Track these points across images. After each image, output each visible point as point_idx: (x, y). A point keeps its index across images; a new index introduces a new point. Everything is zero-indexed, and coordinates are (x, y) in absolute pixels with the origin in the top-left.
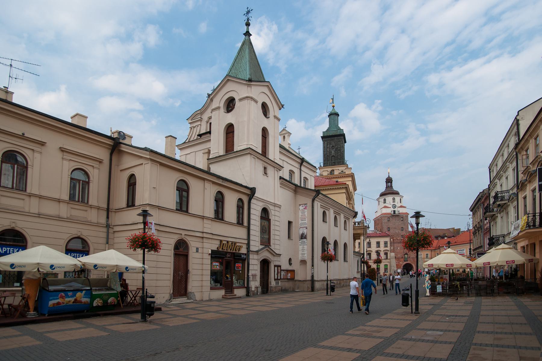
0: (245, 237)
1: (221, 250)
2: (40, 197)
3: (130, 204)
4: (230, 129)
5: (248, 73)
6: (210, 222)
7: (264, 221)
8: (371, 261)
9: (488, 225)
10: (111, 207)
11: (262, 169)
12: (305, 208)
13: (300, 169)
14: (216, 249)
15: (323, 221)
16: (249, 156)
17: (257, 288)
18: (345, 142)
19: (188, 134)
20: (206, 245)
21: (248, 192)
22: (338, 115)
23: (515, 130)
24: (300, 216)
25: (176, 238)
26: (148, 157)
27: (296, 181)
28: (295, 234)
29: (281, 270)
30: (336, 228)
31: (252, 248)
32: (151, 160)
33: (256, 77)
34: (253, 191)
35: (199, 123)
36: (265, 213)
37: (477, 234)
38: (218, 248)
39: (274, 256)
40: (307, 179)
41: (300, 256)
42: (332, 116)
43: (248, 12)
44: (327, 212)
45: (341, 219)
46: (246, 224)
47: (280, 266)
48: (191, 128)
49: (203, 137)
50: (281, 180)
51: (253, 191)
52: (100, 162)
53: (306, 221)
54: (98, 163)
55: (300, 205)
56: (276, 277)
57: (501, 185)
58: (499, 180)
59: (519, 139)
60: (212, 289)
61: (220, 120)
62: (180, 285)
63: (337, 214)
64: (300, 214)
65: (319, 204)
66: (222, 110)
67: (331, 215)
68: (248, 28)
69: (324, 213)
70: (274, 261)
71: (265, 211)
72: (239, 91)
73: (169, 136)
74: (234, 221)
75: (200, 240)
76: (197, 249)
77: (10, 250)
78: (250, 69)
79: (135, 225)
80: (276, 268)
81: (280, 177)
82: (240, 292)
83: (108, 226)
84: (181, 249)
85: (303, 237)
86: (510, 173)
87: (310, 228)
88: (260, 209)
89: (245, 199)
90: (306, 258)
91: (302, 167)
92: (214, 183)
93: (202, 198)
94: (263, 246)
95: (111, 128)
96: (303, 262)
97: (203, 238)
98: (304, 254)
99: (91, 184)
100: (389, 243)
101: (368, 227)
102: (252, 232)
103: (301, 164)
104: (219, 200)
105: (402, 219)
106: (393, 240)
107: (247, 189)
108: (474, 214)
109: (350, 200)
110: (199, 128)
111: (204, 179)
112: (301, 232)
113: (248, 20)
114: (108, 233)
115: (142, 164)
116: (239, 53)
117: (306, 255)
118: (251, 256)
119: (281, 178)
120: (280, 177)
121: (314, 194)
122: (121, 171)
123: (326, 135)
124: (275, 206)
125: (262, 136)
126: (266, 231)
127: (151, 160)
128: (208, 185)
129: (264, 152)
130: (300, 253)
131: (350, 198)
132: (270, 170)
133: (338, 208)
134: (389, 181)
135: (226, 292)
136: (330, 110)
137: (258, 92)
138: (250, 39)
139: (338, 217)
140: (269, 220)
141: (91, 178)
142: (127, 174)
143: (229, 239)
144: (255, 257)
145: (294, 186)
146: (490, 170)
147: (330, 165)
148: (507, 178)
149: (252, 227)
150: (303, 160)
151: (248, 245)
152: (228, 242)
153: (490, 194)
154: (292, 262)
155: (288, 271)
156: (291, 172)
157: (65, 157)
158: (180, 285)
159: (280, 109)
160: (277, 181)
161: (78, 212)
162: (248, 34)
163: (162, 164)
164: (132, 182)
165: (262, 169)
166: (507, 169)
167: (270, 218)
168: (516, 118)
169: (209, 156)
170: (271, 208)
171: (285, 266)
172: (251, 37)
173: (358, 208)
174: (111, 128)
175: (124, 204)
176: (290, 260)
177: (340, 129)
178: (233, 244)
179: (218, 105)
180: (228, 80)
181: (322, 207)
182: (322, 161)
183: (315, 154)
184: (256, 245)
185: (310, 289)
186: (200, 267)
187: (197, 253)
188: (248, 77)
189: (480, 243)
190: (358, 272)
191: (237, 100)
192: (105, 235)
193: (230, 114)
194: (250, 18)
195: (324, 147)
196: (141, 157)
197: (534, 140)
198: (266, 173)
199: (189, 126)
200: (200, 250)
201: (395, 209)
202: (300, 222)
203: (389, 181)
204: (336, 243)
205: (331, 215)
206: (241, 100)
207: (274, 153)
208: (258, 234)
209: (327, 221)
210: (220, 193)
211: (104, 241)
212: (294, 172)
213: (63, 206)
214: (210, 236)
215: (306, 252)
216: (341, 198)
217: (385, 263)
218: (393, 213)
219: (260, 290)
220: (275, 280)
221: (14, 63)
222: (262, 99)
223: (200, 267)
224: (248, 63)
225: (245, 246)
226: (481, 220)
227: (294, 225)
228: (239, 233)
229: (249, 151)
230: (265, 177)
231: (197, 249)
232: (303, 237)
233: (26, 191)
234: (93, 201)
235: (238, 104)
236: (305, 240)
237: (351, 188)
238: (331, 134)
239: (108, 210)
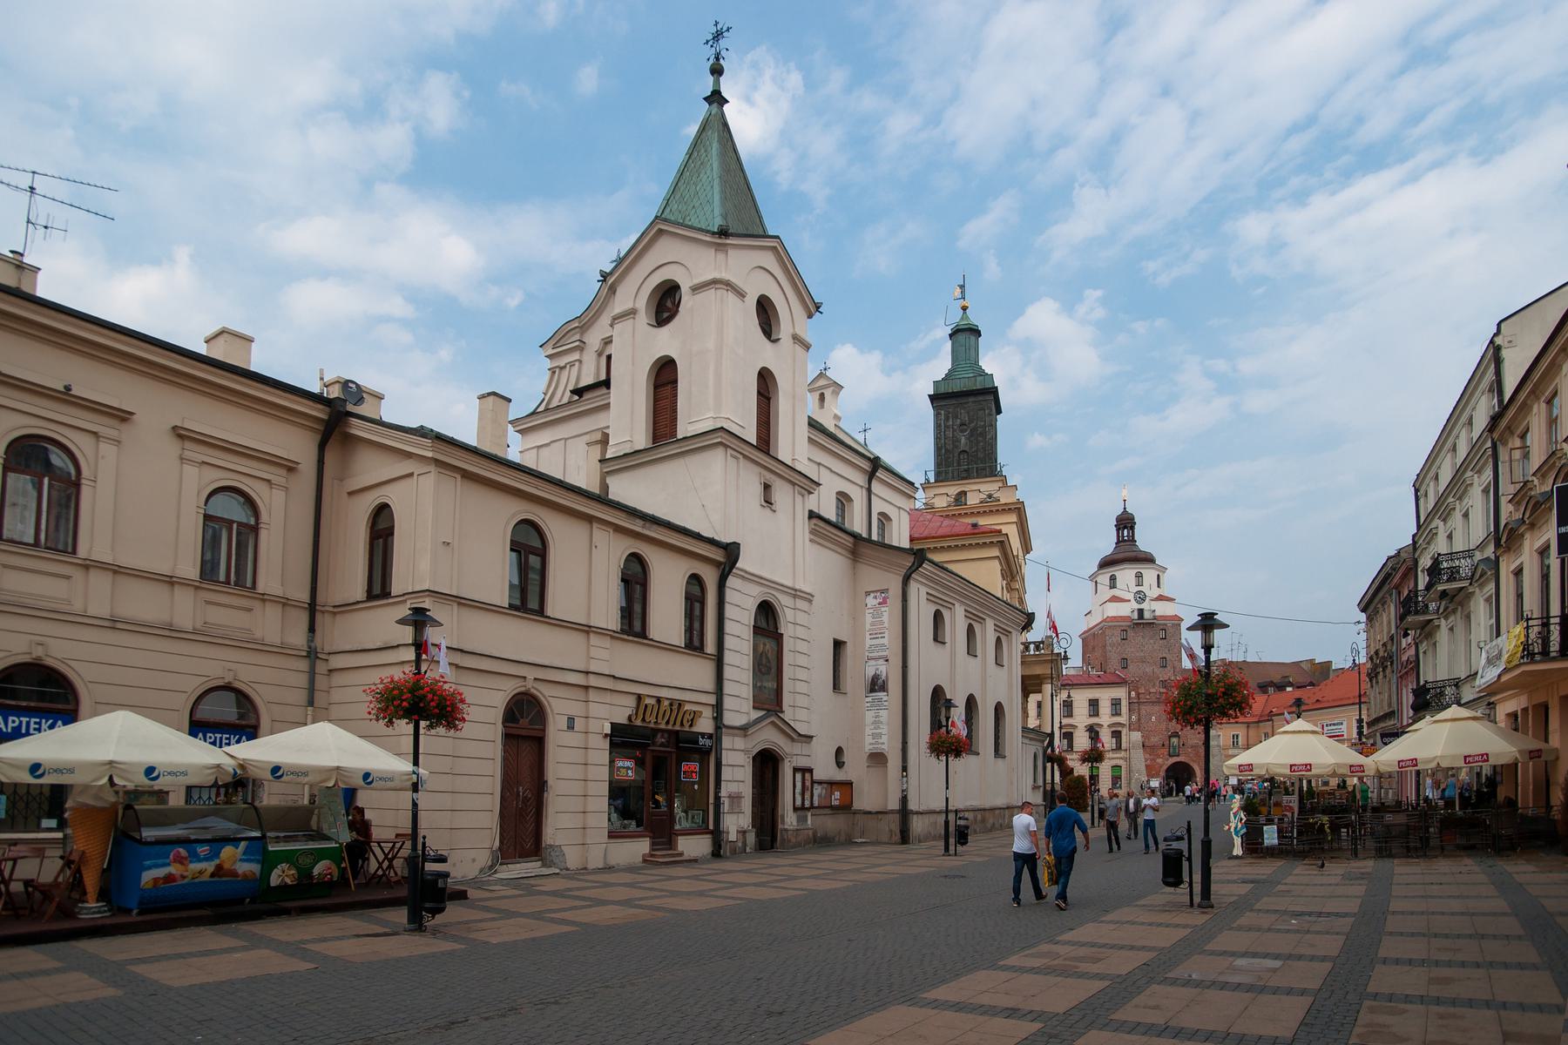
0: (709, 685)
1: (638, 723)
2: (117, 570)
3: (377, 590)
4: (665, 374)
5: (717, 212)
6: (607, 642)
8: (1075, 756)
9: (1412, 651)
10: (320, 599)
11: (758, 490)
12: (884, 602)
13: (869, 491)
14: (625, 721)
15: (936, 639)
16: (720, 451)
17: (744, 832)
18: (999, 411)
19: (543, 387)
20: (595, 709)
21: (718, 555)
22: (977, 333)
24: (868, 627)
25: (510, 688)
26: (430, 454)
28: (855, 678)
29: (813, 782)
30: (971, 659)
31: (730, 719)
32: (437, 462)
33: (741, 222)
34: (731, 552)
35: (576, 356)
37: (1380, 676)
38: (630, 718)
40: (888, 518)
41: (869, 740)
42: (961, 337)
43: (718, 36)
44: (946, 613)
45: (987, 634)
46: (710, 647)
47: (811, 771)
48: (553, 371)
49: (587, 396)
50: (815, 521)
51: (731, 552)
52: (291, 468)
53: (885, 641)
54: (283, 472)
55: (868, 593)
56: (799, 803)
57: (1450, 537)
58: (1444, 520)
60: (612, 835)
61: (636, 348)
62: (522, 824)
63: (973, 620)
64: (869, 619)
65: (924, 590)
66: (644, 318)
67: (957, 622)
68: (717, 83)
69: (938, 616)
70: (793, 756)
71: (766, 611)
72: (690, 264)
74: (678, 639)
75: (580, 694)
76: (571, 720)
77: (28, 724)
78: (724, 199)
79: (390, 652)
80: (799, 776)
81: (811, 512)
82: (693, 846)
83: (312, 655)
84: (524, 722)
85: (876, 685)
86: (1476, 501)
87: (896, 661)
88: (752, 605)
89: (710, 577)
90: (885, 748)
92: (618, 529)
94: (761, 713)
95: (321, 371)
96: (878, 758)
97: (586, 688)
98: (880, 735)
99: (263, 534)
100: (1124, 703)
101: (1066, 658)
102: (728, 672)
103: (871, 476)
104: (635, 579)
106: (1138, 694)
107: (714, 548)
108: (1370, 619)
110: (575, 369)
111: (590, 519)
112: (870, 672)
113: (717, 59)
114: (312, 674)
115: (411, 475)
117: (884, 739)
118: (727, 742)
119: (812, 515)
120: (811, 512)
121: (908, 561)
122: (350, 494)
123: (942, 390)
124: (795, 596)
125: (759, 393)
126: (770, 669)
127: (437, 462)
128: (601, 536)
129: (765, 441)
130: (868, 731)
131: (1011, 572)
132: (782, 493)
133: (979, 602)
134: (1125, 523)
135: (653, 844)
136: (955, 317)
137: (745, 267)
139: (977, 627)
140: (778, 638)
141: (264, 517)
142: (368, 502)
143: (663, 693)
144: (739, 743)
145: (851, 539)
146: (1417, 491)
147: (953, 479)
148: (1466, 515)
149: (729, 657)
150: (876, 464)
151: (718, 708)
152: (659, 700)
153: (1416, 562)
155: (832, 784)
156: (843, 499)
157: (187, 454)
158: (522, 824)
159: (810, 316)
160: (803, 525)
161: (226, 613)
162: (716, 98)
163: (467, 476)
164: (381, 528)
165: (759, 489)
166: (1465, 491)
167: (782, 631)
169: (604, 451)
170: (783, 602)
171: (824, 769)
172: (726, 108)
174: (321, 371)
175: (359, 592)
176: (839, 751)
177: (982, 373)
178: (675, 707)
179: (630, 305)
180: (661, 231)
181: (931, 598)
183: (911, 447)
184: (739, 708)
185: (897, 837)
186: (580, 774)
187: (570, 734)
188: (717, 223)
189: (1390, 705)
190: (1035, 788)
191: (685, 288)
192: (303, 680)
193: (665, 330)
194: (724, 53)
195: (937, 426)
196: (409, 455)
198: (768, 502)
199: (548, 364)
200: (578, 724)
201: (1144, 606)
202: (868, 642)
203: (1125, 523)
204: (971, 703)
205: (957, 622)
206: (696, 289)
207: (792, 444)
209: (947, 640)
210: (635, 558)
211: (301, 696)
212: (849, 499)
213: (184, 598)
214: (609, 684)
215: (884, 730)
216: (986, 573)
218: (1136, 616)
219: (751, 838)
220: (795, 809)
221: (39, 184)
222: (758, 285)
223: (580, 774)
224: (716, 182)
225: (708, 713)
226: (1392, 638)
227: (849, 650)
228: (692, 675)
229: (720, 438)
231: (571, 720)
232: (876, 685)
233: (74, 552)
234: (268, 581)
235: (687, 300)
236: (881, 694)
238: (957, 387)
239: (312, 608)
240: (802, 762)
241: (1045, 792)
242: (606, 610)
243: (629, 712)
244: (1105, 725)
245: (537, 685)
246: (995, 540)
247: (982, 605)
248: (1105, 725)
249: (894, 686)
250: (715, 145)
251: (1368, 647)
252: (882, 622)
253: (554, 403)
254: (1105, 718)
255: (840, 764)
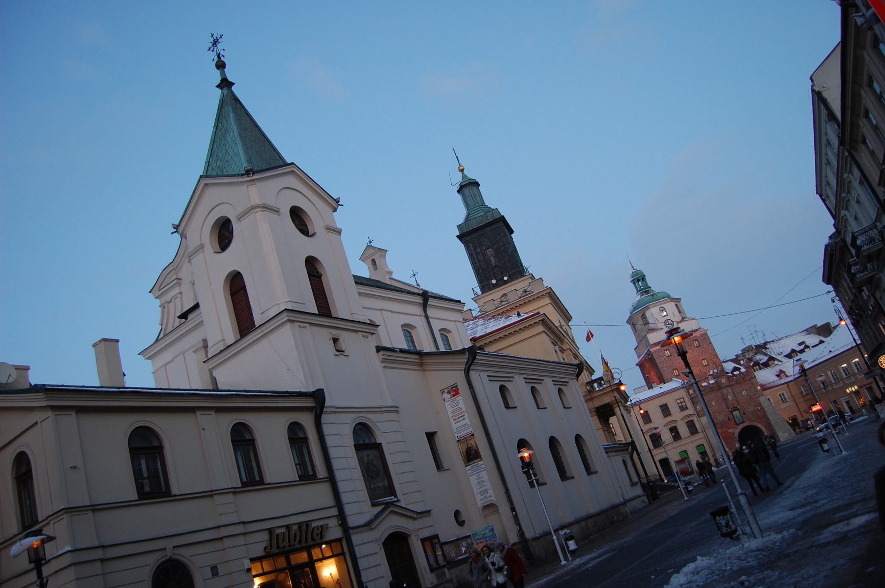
0: (329, 501)
2: (95, 508)
4: (236, 285)
5: (243, 159)
7: (366, 452)
9: (872, 300)
12: (457, 393)
13: (427, 317)
15: (507, 407)
16: (288, 326)
18: (512, 232)
21: (309, 403)
22: (476, 184)
23: (824, 112)
24: (450, 415)
25: (151, 562)
26: (44, 404)
27: (427, 346)
28: (452, 454)
31: (352, 521)
32: (54, 408)
33: (265, 160)
34: (318, 396)
35: (176, 290)
36: (365, 441)
37: (861, 323)
39: (414, 519)
40: (449, 331)
41: (478, 497)
42: (466, 191)
43: (215, 43)
46: (322, 472)
47: (437, 536)
48: (163, 306)
49: (190, 317)
50: (382, 353)
51: (318, 396)
57: (856, 218)
58: (847, 209)
59: (838, 125)
65: (484, 375)
67: (519, 388)
68: (223, 73)
69: (503, 389)
70: (417, 531)
71: (363, 431)
72: (230, 199)
73: (101, 341)
74: (291, 473)
78: (246, 149)
79: (136, 545)
80: (428, 545)
86: (859, 191)
88: (348, 430)
89: (307, 421)
91: (429, 310)
92: (218, 410)
93: (197, 453)
94: (379, 509)
96: (490, 507)
102: (342, 487)
103: (425, 305)
104: (243, 441)
105: (696, 344)
108: (836, 289)
109: (562, 341)
110: (178, 301)
111: (192, 410)
115: (36, 423)
116: (216, 126)
117: (491, 492)
118: (356, 539)
121: (464, 359)
125: (309, 275)
127: (54, 408)
129: (324, 308)
131: (558, 337)
132: (348, 340)
133: (534, 370)
134: (639, 279)
136: (458, 179)
137: (271, 190)
138: (232, 93)
142: (10, 453)
145: (417, 357)
146: (821, 196)
148: (858, 202)
149: (339, 475)
150: (425, 296)
151: (342, 517)
152: (288, 527)
153: (844, 241)
154: (464, 517)
155: (457, 542)
156: (407, 329)
159: (335, 210)
160: (376, 359)
162: (225, 84)
163: (80, 410)
166: (849, 187)
167: (380, 439)
168: (813, 91)
169: (206, 353)
170: (376, 421)
171: (448, 531)
172: (233, 88)
173: (590, 353)
176: (457, 514)
177: (489, 210)
178: (304, 527)
180: (206, 185)
181: (492, 379)
182: (474, 282)
183: (453, 274)
188: (245, 165)
189: (877, 340)
190: (633, 484)
194: (222, 53)
195: (471, 256)
197: (864, 120)
199: (158, 302)
202: (455, 426)
203: (639, 279)
205: (519, 388)
206: (239, 219)
207: (346, 302)
208: (361, 484)
214: (240, 529)
215: (488, 485)
216: (537, 347)
217: (697, 443)
220: (432, 570)
222: (286, 203)
224: (238, 139)
225: (333, 523)
226: (855, 296)
228: (317, 496)
230: (342, 357)
232: (471, 455)
237: (555, 318)
240: (426, 533)
241: (643, 485)
242: (224, 469)
243: (264, 544)
244: (679, 419)
245: (177, 551)
246: (537, 320)
247: (535, 370)
248: (679, 419)
249: (484, 450)
250: (232, 115)
251: (844, 306)
252: (460, 409)
253: (170, 329)
254: (677, 415)
255: (461, 523)
